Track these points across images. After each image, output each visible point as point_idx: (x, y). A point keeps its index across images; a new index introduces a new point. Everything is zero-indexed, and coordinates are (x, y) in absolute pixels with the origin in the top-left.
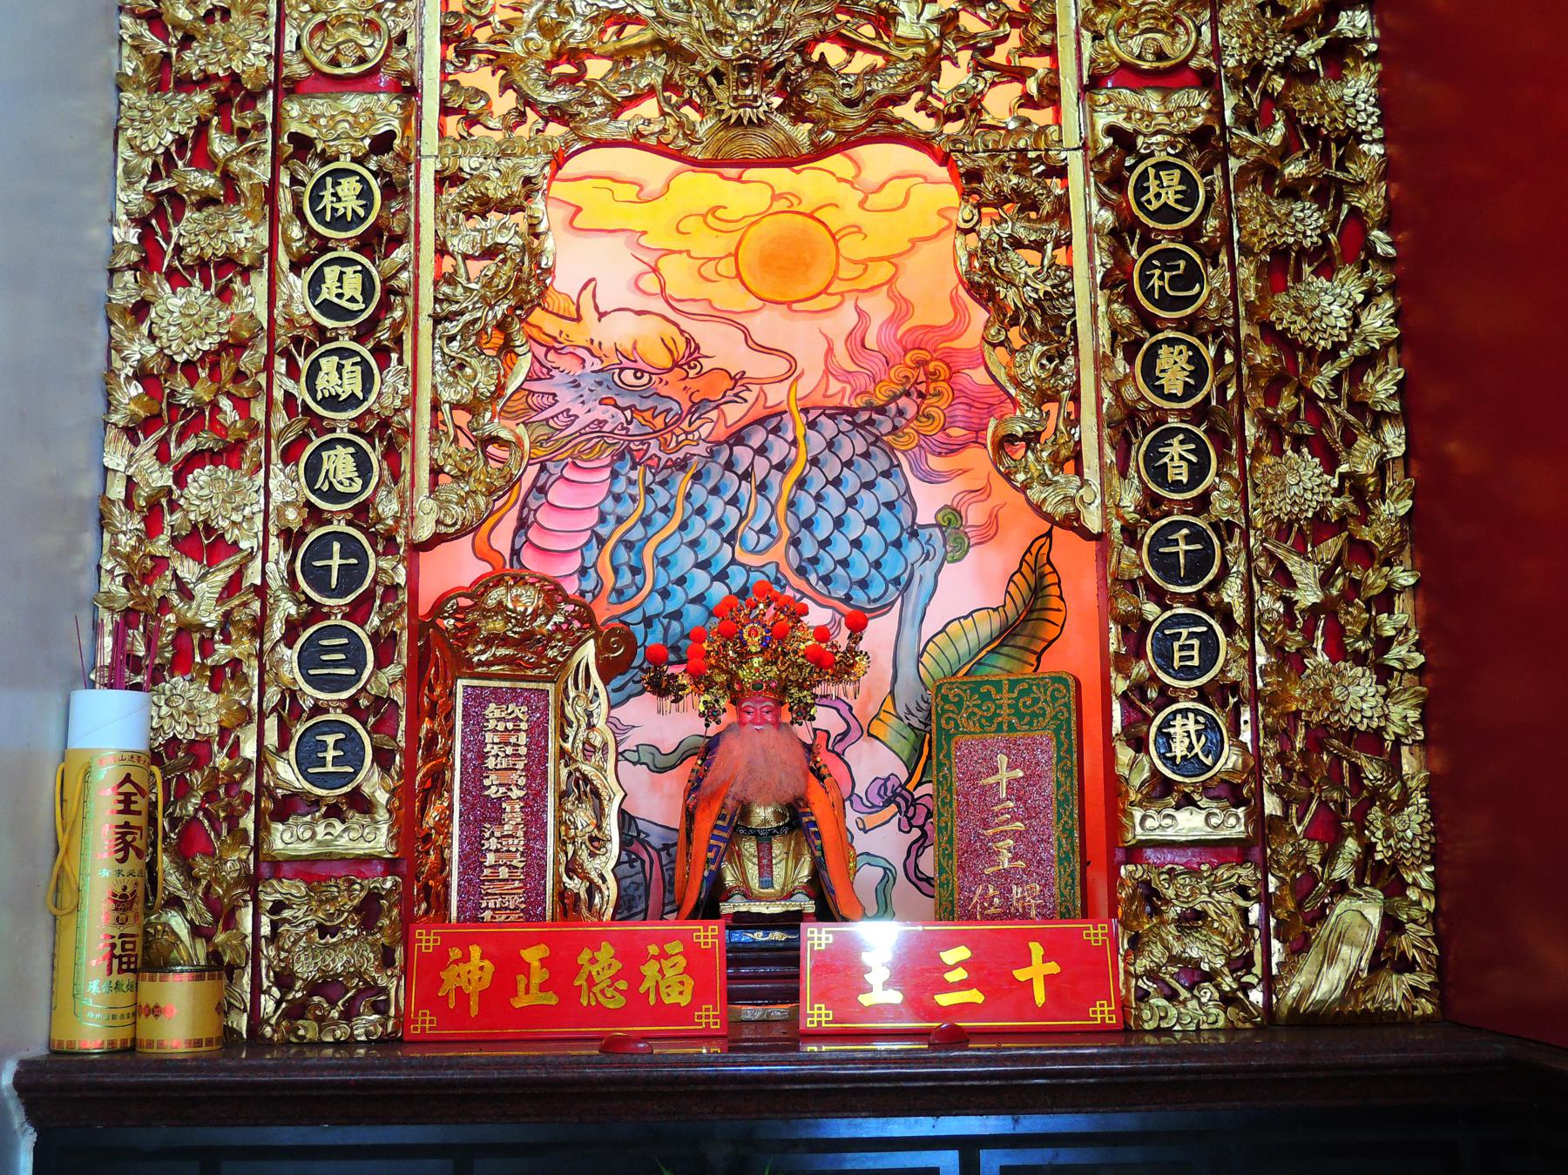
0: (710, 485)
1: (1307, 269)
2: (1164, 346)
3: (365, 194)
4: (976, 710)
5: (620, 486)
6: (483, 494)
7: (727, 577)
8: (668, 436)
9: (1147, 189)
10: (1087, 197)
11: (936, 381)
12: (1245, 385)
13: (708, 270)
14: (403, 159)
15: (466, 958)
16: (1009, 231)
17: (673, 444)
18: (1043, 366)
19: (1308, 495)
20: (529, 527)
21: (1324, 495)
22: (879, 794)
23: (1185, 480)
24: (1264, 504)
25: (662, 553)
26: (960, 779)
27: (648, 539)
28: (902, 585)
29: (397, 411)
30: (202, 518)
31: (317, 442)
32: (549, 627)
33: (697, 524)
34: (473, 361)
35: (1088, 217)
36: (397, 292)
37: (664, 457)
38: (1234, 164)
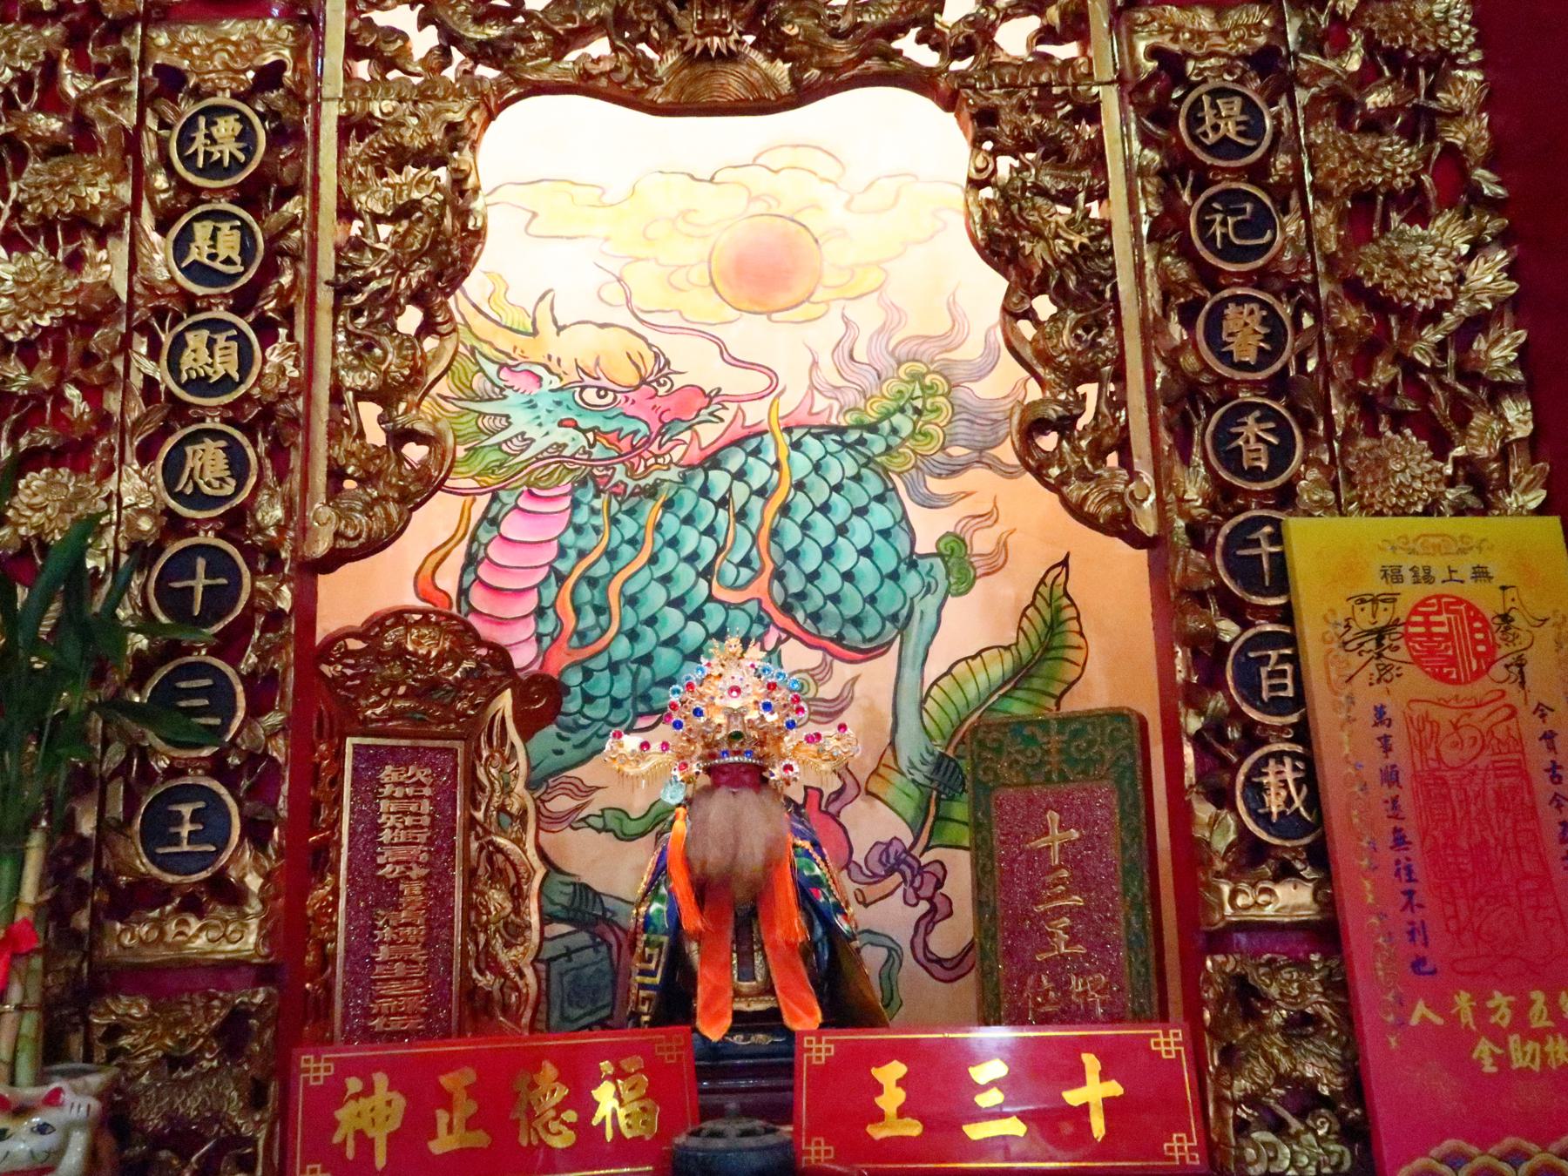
0: (683, 514)
1: (1395, 217)
2: (1232, 306)
3: (246, 136)
4: (1019, 757)
5: (582, 516)
6: (394, 500)
7: (703, 615)
8: (635, 460)
9: (1202, 120)
10: (1125, 137)
11: (934, 395)
12: (1329, 353)
13: (678, 279)
14: (296, 97)
15: (368, 1090)
16: (1032, 179)
17: (641, 469)
18: (1078, 337)
19: (1418, 485)
20: (480, 563)
21: (1436, 483)
22: (880, 860)
23: (1264, 466)
24: (1361, 497)
25: (631, 589)
26: (1003, 843)
27: (613, 575)
28: (900, 621)
29: (283, 396)
30: (33, 533)
31: (180, 434)
32: (458, 674)
33: (669, 558)
34: (385, 340)
35: (1128, 161)
36: (283, 253)
37: (631, 484)
38: (1302, 96)
